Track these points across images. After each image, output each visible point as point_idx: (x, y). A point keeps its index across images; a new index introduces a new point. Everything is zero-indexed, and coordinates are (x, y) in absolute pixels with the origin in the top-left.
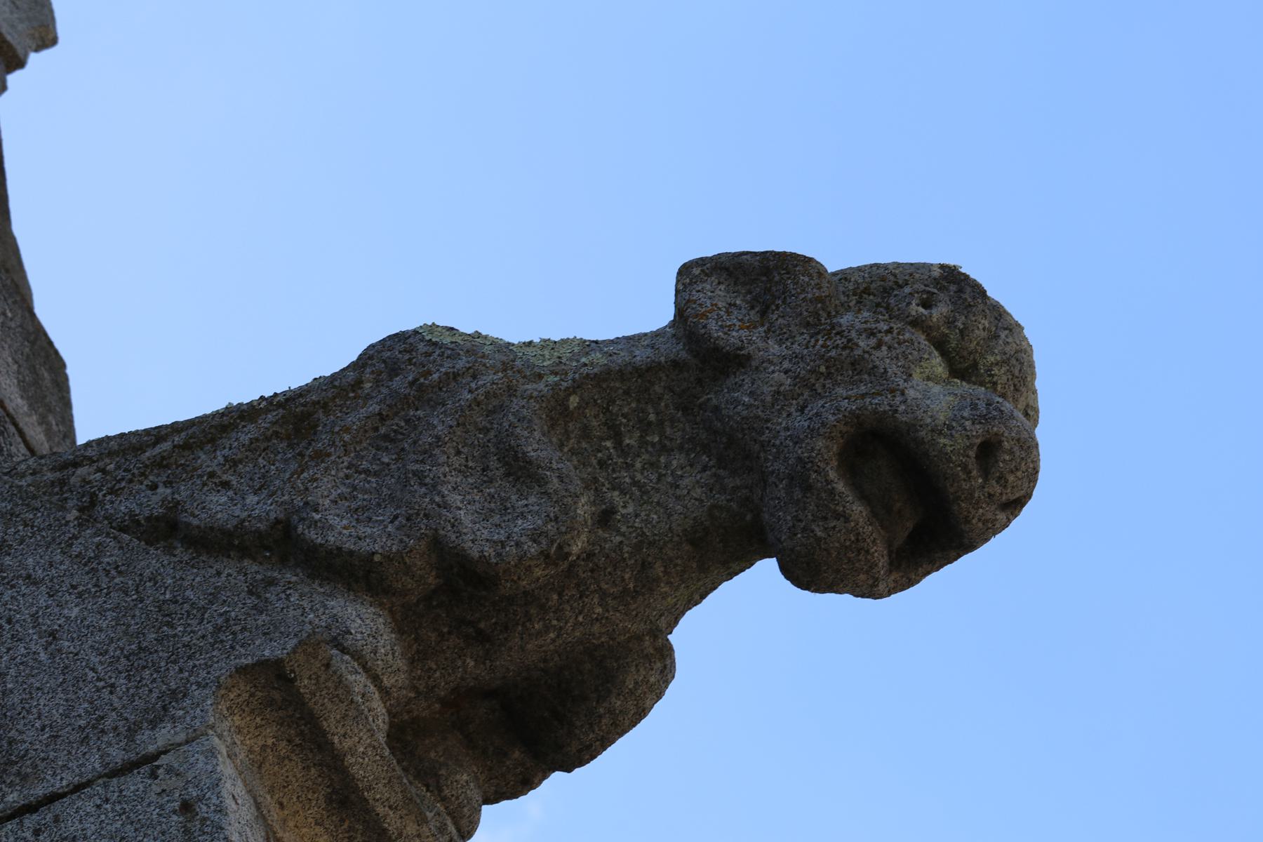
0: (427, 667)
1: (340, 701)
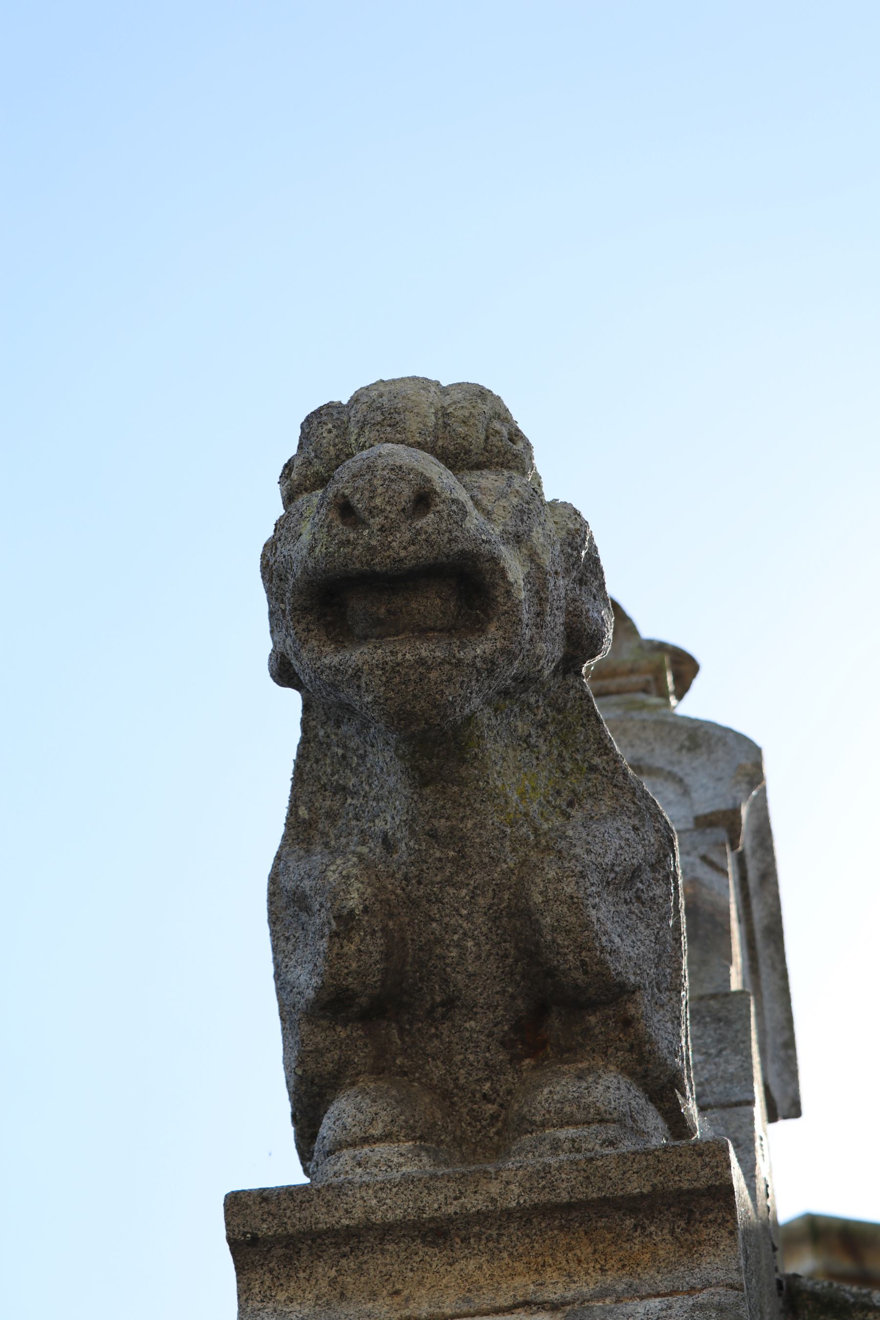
0: (459, 1063)
1: (308, 1202)
